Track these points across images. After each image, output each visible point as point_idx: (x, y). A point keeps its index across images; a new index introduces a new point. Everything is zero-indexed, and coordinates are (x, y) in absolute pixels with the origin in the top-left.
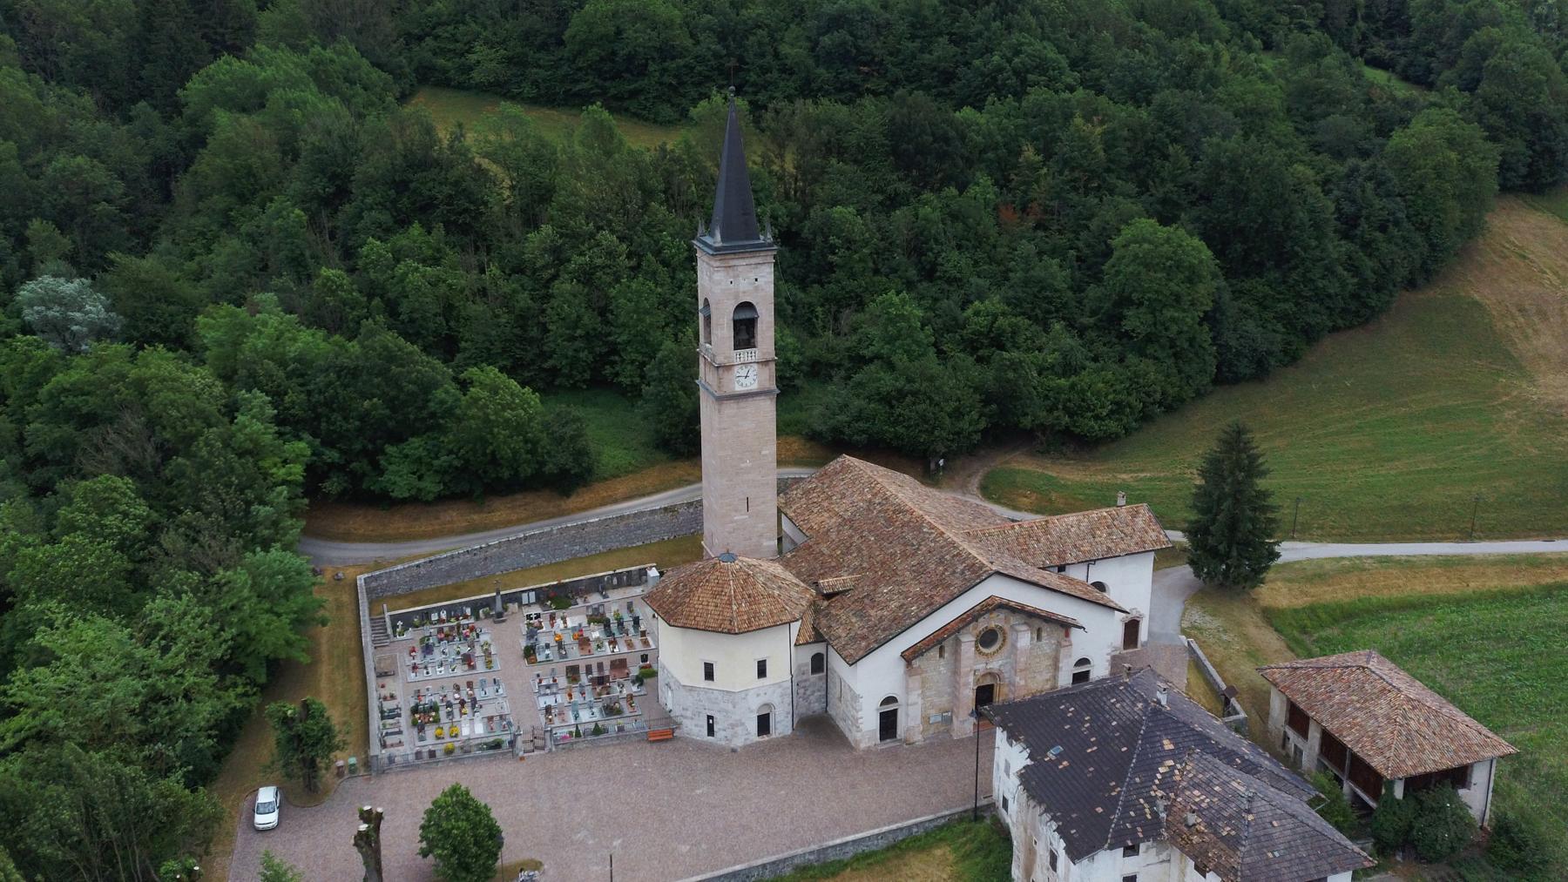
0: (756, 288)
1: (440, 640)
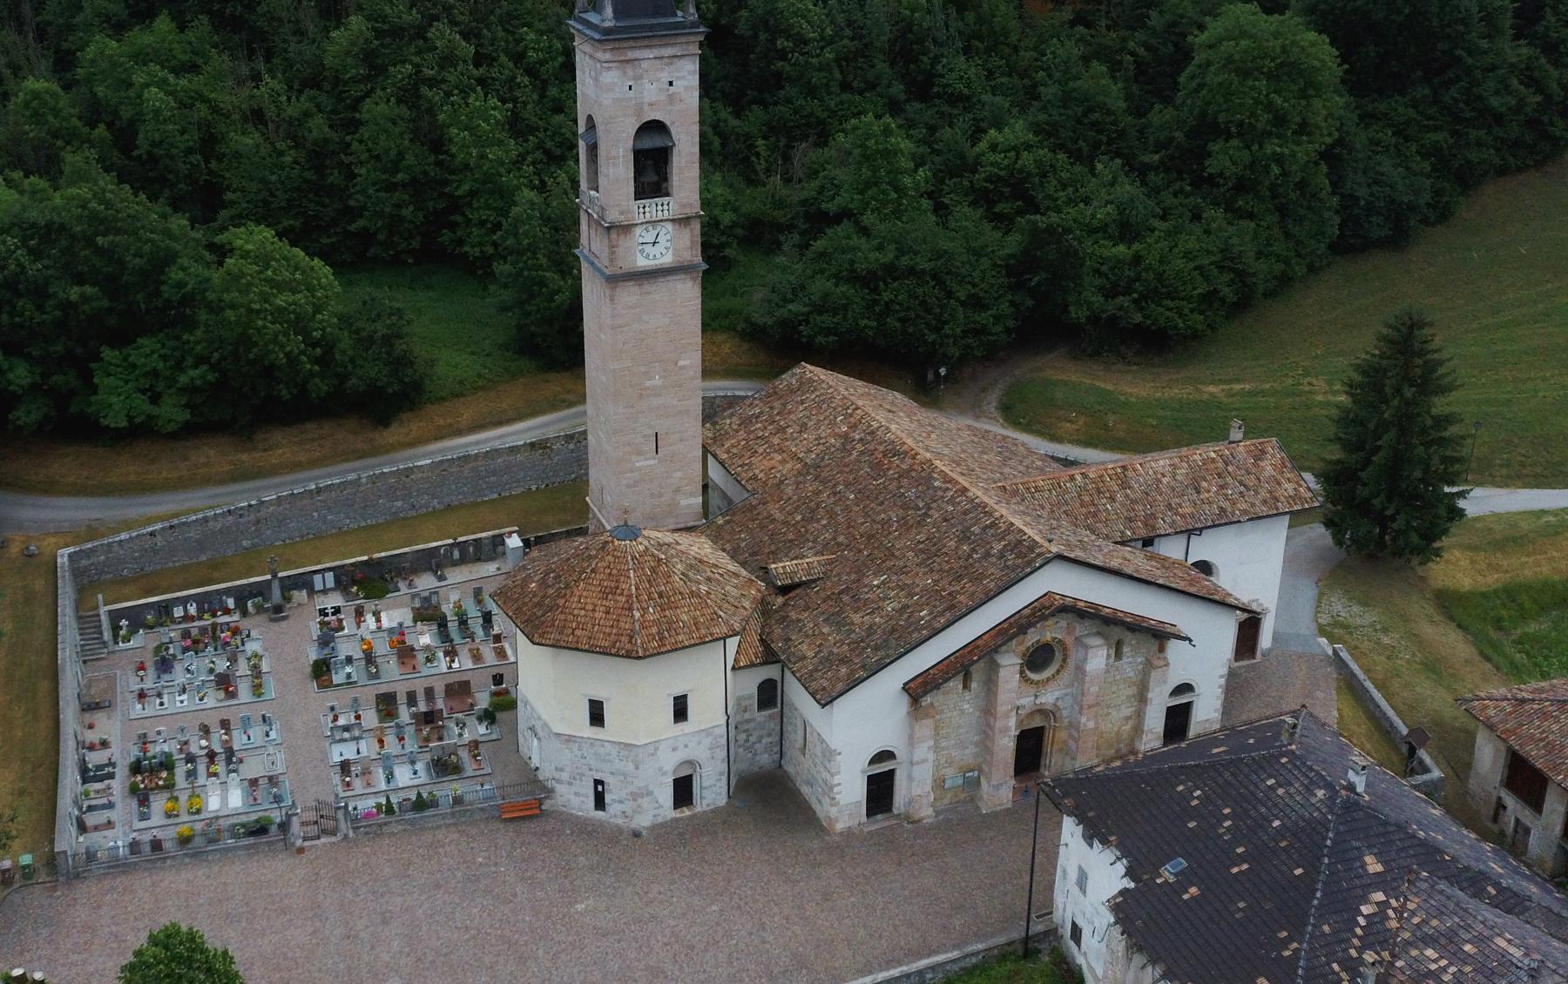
0: (671, 98)
1: (185, 650)
